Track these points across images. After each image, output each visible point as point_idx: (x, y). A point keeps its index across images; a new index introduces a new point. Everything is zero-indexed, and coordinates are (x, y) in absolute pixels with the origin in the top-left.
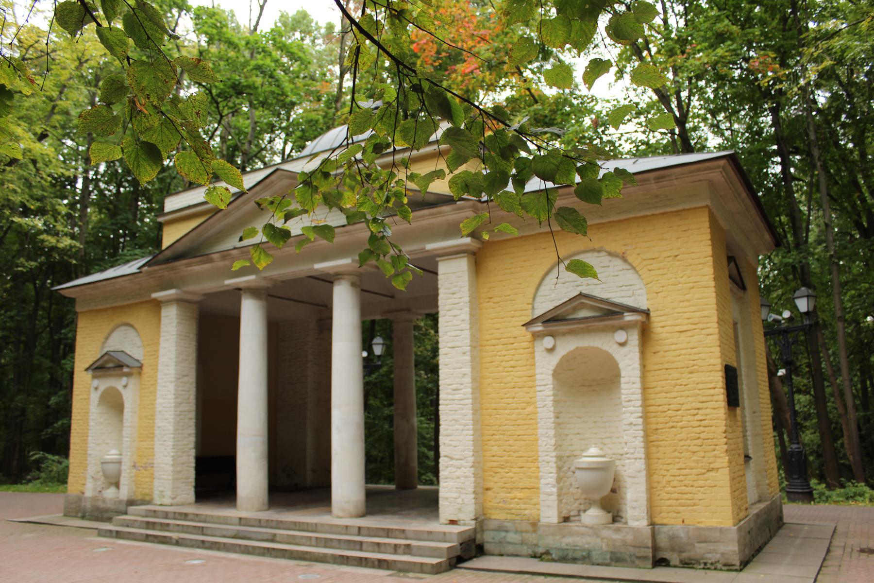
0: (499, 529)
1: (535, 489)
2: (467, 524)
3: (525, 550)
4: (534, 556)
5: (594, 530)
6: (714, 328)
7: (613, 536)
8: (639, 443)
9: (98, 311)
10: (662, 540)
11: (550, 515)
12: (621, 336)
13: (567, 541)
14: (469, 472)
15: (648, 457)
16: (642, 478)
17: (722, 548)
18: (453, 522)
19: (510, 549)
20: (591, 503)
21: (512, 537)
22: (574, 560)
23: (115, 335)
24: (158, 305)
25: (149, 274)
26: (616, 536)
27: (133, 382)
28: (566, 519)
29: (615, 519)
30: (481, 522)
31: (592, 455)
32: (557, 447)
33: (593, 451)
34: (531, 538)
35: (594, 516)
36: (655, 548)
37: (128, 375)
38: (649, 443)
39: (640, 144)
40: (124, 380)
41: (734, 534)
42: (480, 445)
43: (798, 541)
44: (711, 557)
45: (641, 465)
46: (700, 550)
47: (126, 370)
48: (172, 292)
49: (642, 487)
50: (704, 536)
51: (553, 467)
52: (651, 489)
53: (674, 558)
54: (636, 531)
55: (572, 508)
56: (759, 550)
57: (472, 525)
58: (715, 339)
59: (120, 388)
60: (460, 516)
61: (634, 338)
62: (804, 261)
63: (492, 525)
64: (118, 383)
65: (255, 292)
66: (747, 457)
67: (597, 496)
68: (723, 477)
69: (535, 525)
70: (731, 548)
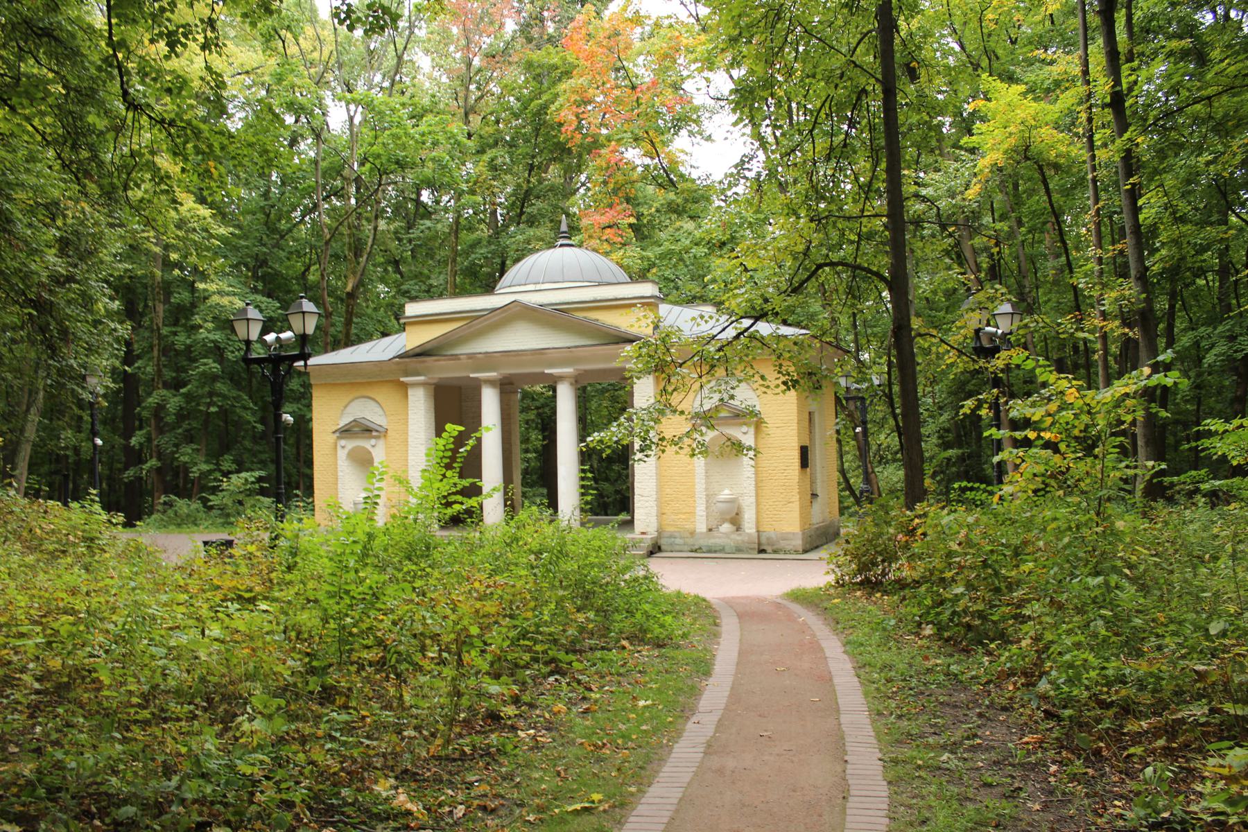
0: (671, 537)
1: (693, 513)
2: (652, 533)
3: (686, 548)
4: (692, 551)
5: (727, 535)
6: (795, 426)
7: (737, 537)
8: (752, 488)
9: (335, 385)
10: (763, 540)
11: (702, 527)
12: (744, 429)
13: (711, 542)
14: (653, 504)
15: (757, 495)
16: (753, 507)
17: (794, 543)
18: (643, 533)
19: (677, 548)
20: (724, 521)
21: (678, 541)
22: (715, 552)
23: (353, 404)
24: (405, 386)
25: (398, 363)
26: (739, 538)
27: (381, 444)
28: (710, 530)
29: (738, 529)
30: (660, 532)
31: (726, 494)
32: (707, 489)
33: (727, 492)
34: (690, 541)
35: (726, 527)
36: (759, 544)
37: (377, 437)
38: (757, 487)
39: (785, 159)
40: (373, 442)
41: (800, 536)
42: (660, 489)
43: (639, 456)
44: (788, 548)
45: (753, 499)
46: (783, 544)
47: (374, 434)
48: (422, 378)
49: (753, 512)
50: (785, 537)
51: (703, 501)
52: (758, 513)
53: (769, 549)
54: (749, 534)
55: (713, 524)
56: (817, 547)
57: (655, 534)
58: (795, 432)
59: (368, 447)
60: (648, 530)
61: (752, 430)
62: (464, 732)
63: (666, 534)
64: (366, 444)
65: (491, 382)
66: (814, 495)
67: (728, 517)
68: (796, 506)
69: (692, 533)
70: (798, 543)
